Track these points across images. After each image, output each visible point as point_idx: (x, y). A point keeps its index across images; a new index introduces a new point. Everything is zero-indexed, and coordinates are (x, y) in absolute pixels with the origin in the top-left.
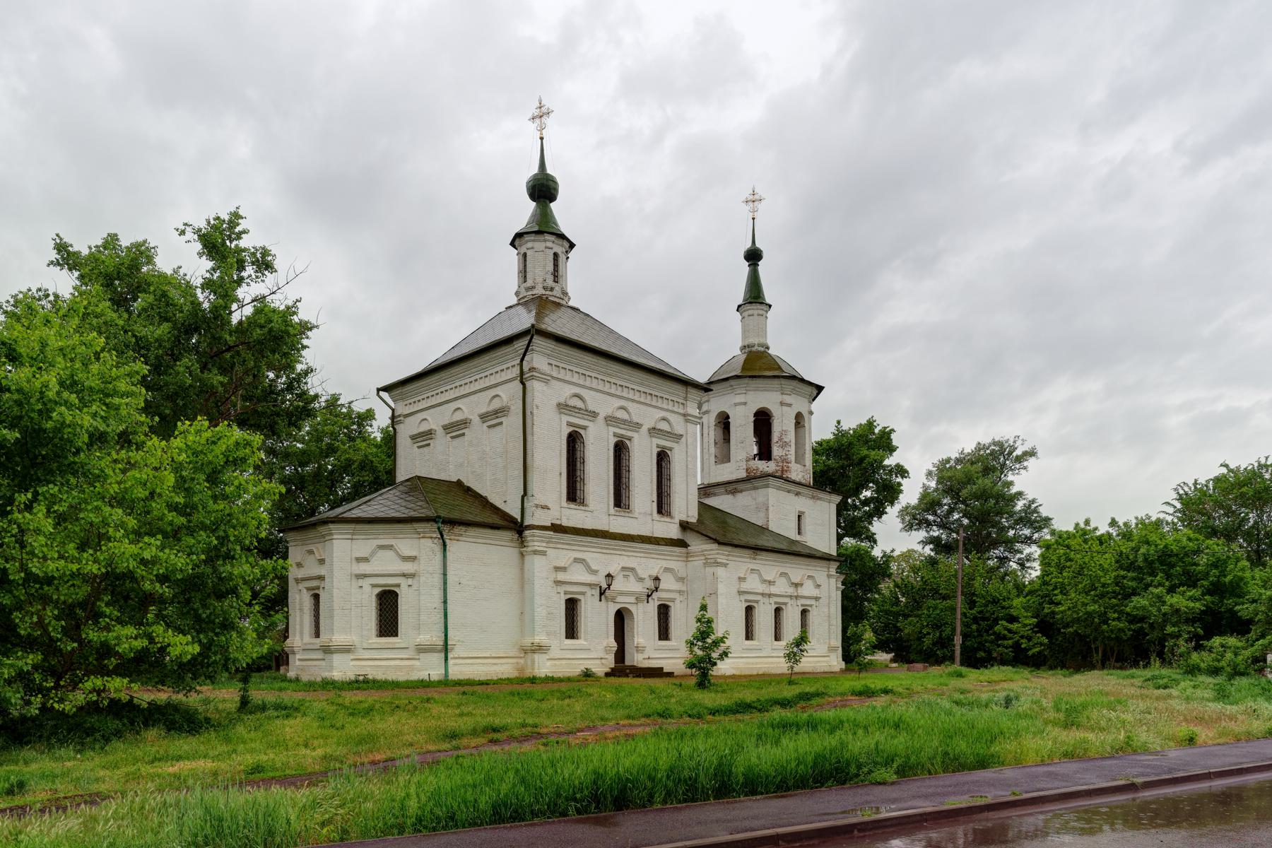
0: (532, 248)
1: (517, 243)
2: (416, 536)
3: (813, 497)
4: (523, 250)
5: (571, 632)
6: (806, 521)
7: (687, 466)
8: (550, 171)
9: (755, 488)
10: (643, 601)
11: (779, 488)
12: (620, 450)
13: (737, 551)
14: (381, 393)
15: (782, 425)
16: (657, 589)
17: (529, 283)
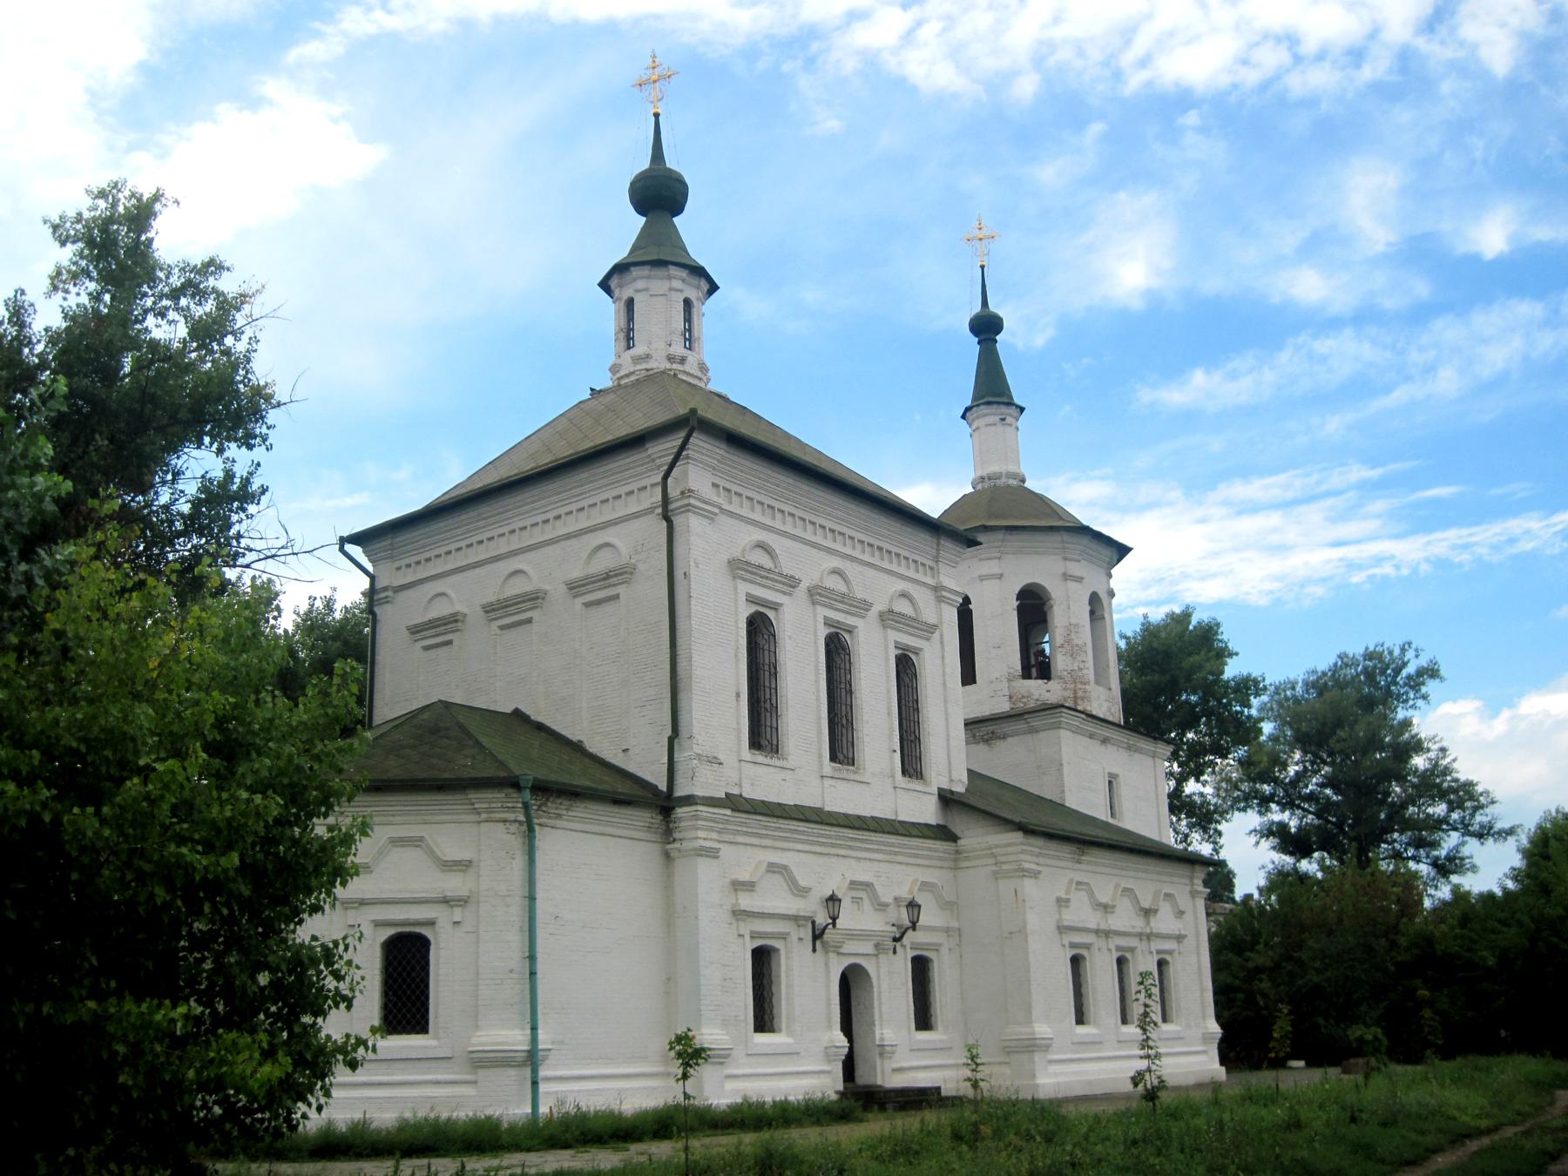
0: (647, 290)
1: (613, 283)
2: (473, 817)
3: (1129, 748)
4: (627, 293)
5: (764, 1020)
6: (1123, 790)
7: (944, 684)
8: (671, 162)
9: (1033, 731)
10: (885, 951)
11: (1077, 731)
12: (837, 650)
13: (1054, 848)
14: (349, 548)
15: (1068, 612)
16: (914, 926)
17: (639, 350)
